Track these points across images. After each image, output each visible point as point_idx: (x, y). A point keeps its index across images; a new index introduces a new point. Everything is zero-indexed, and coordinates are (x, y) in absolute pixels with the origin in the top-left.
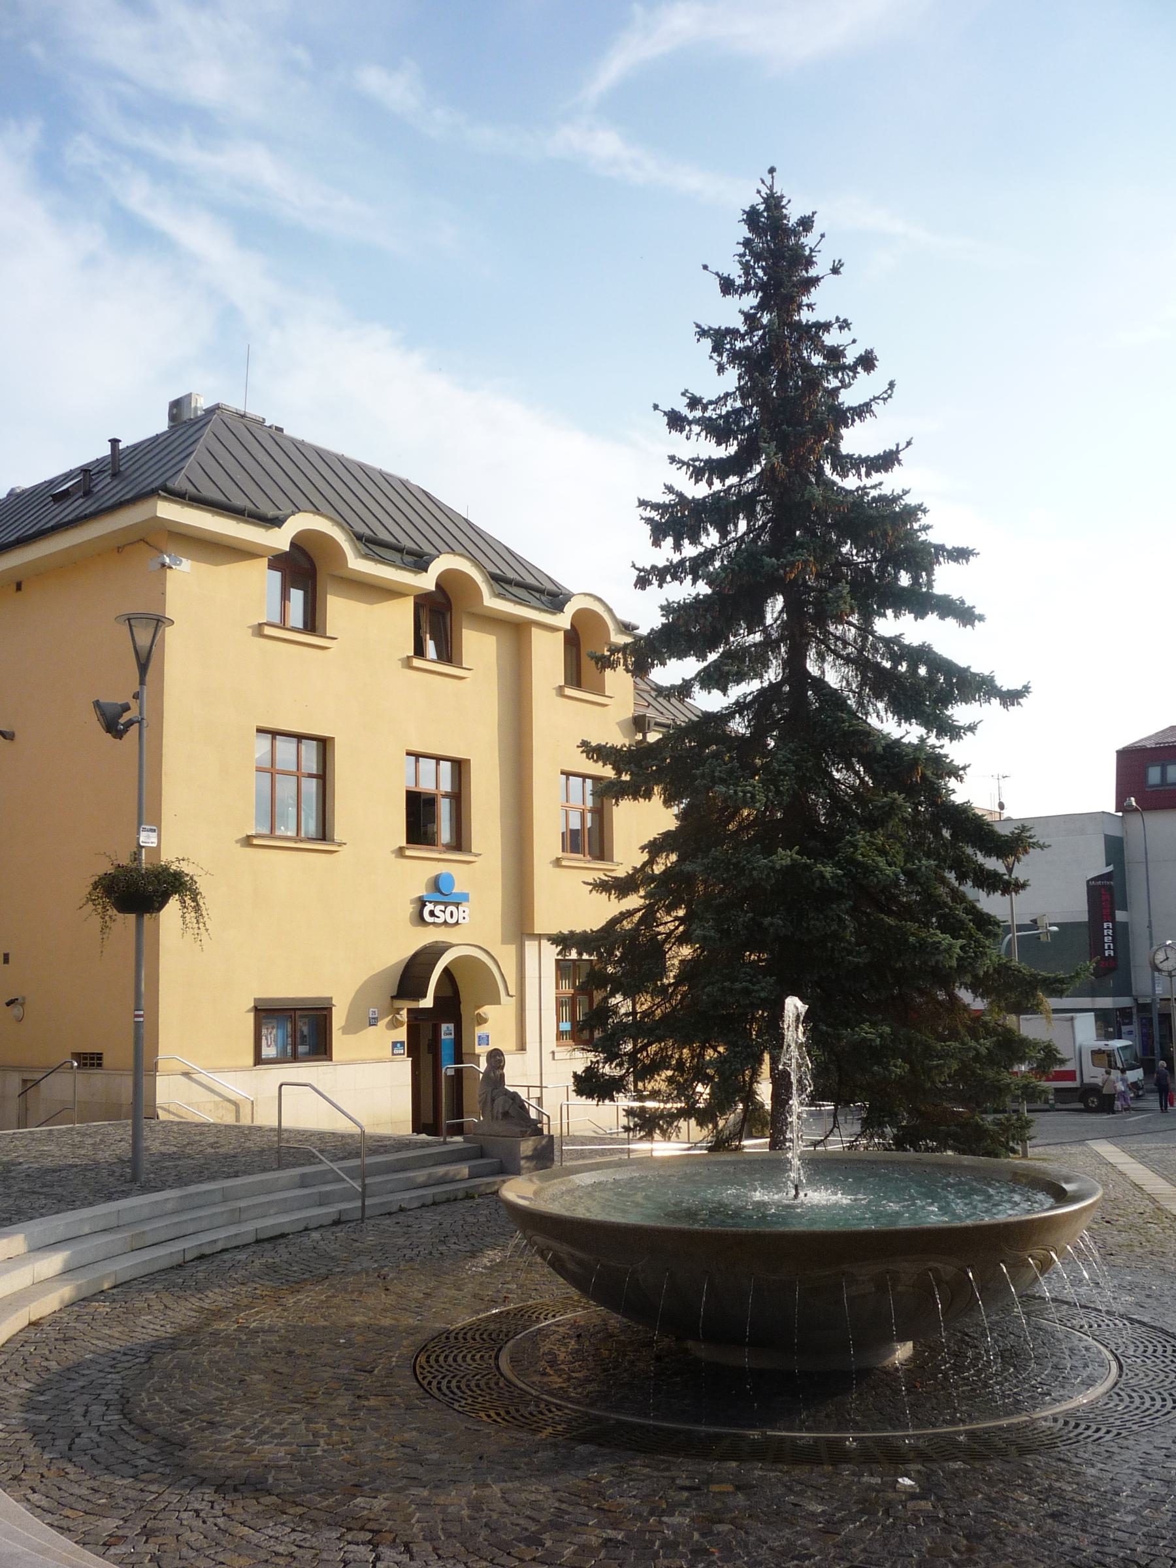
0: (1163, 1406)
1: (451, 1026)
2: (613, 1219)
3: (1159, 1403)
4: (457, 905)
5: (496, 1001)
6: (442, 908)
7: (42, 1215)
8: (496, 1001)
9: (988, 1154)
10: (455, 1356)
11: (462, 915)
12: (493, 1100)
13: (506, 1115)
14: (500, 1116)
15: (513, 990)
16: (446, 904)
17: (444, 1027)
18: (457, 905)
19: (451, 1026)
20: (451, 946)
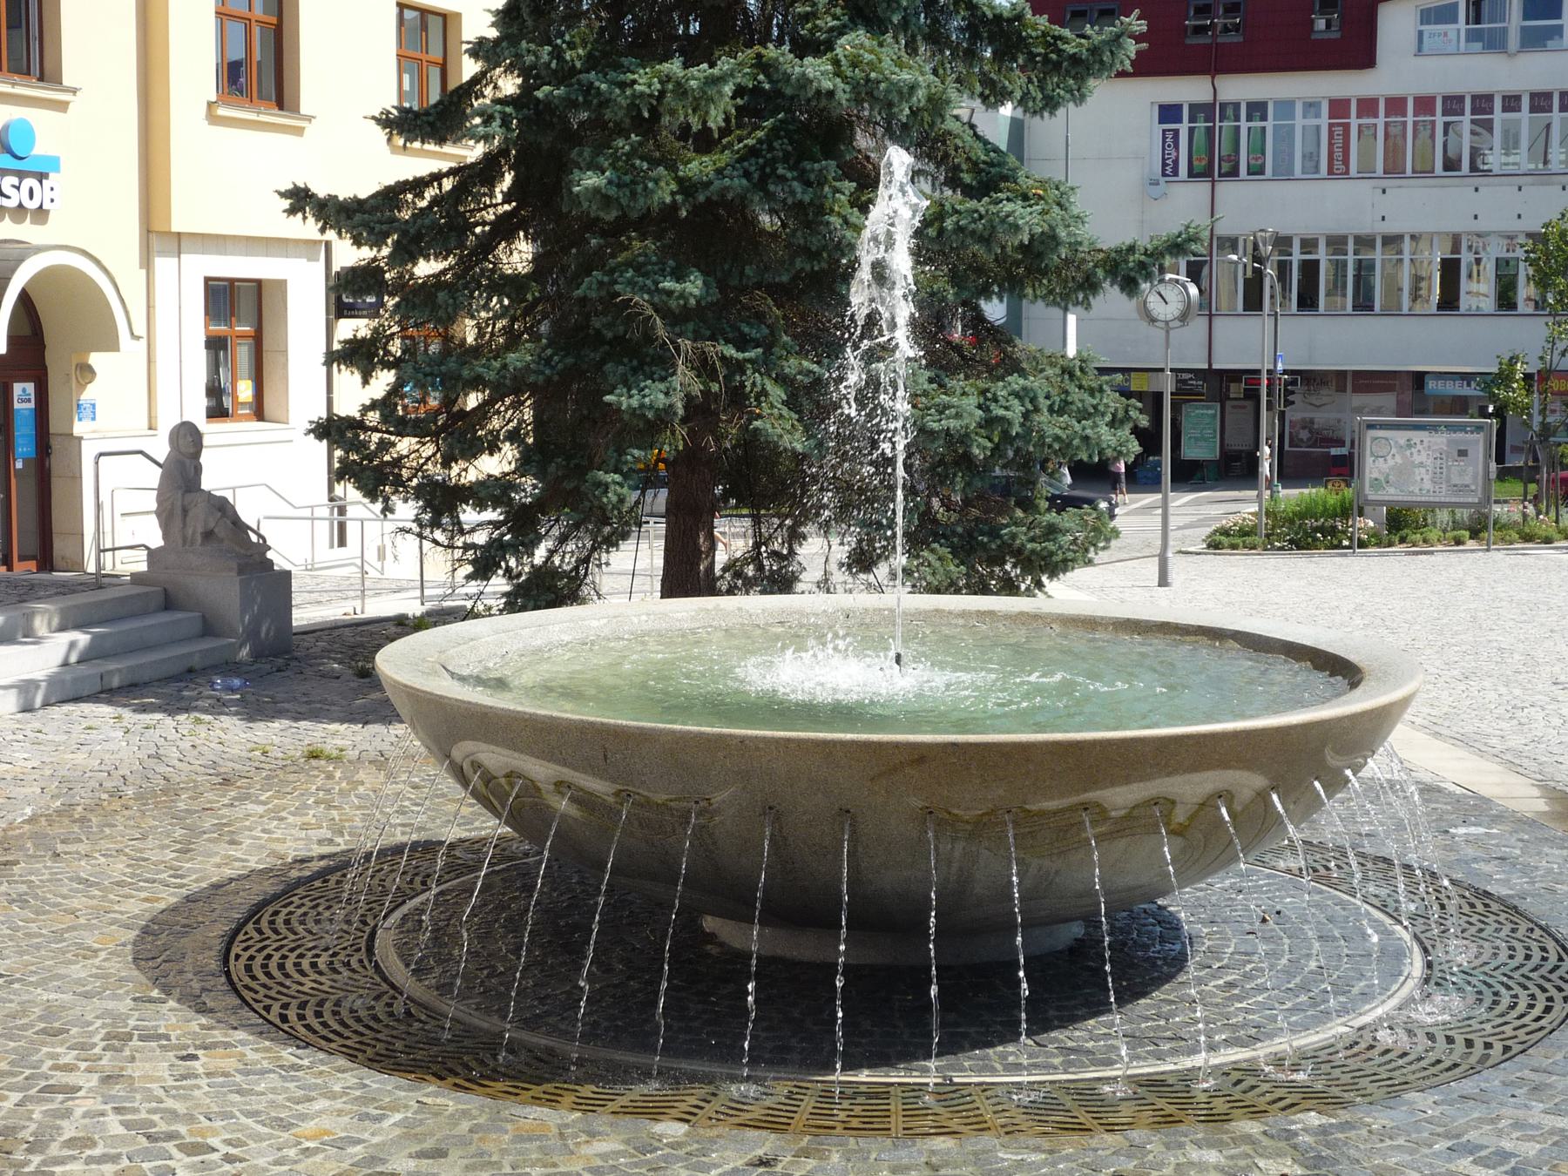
0: (1544, 959)
1: (30, 387)
2: (520, 709)
3: (305, 964)
4: (41, 177)
5: (112, 345)
6: (15, 181)
7: (1234, 547)
8: (112, 345)
9: (1009, 588)
10: (1513, 1007)
11: (48, 195)
12: (185, 511)
13: (208, 535)
14: (199, 539)
15: (140, 329)
16: (21, 175)
17: (18, 388)
18: (41, 177)
19: (30, 387)
20: (39, 249)
